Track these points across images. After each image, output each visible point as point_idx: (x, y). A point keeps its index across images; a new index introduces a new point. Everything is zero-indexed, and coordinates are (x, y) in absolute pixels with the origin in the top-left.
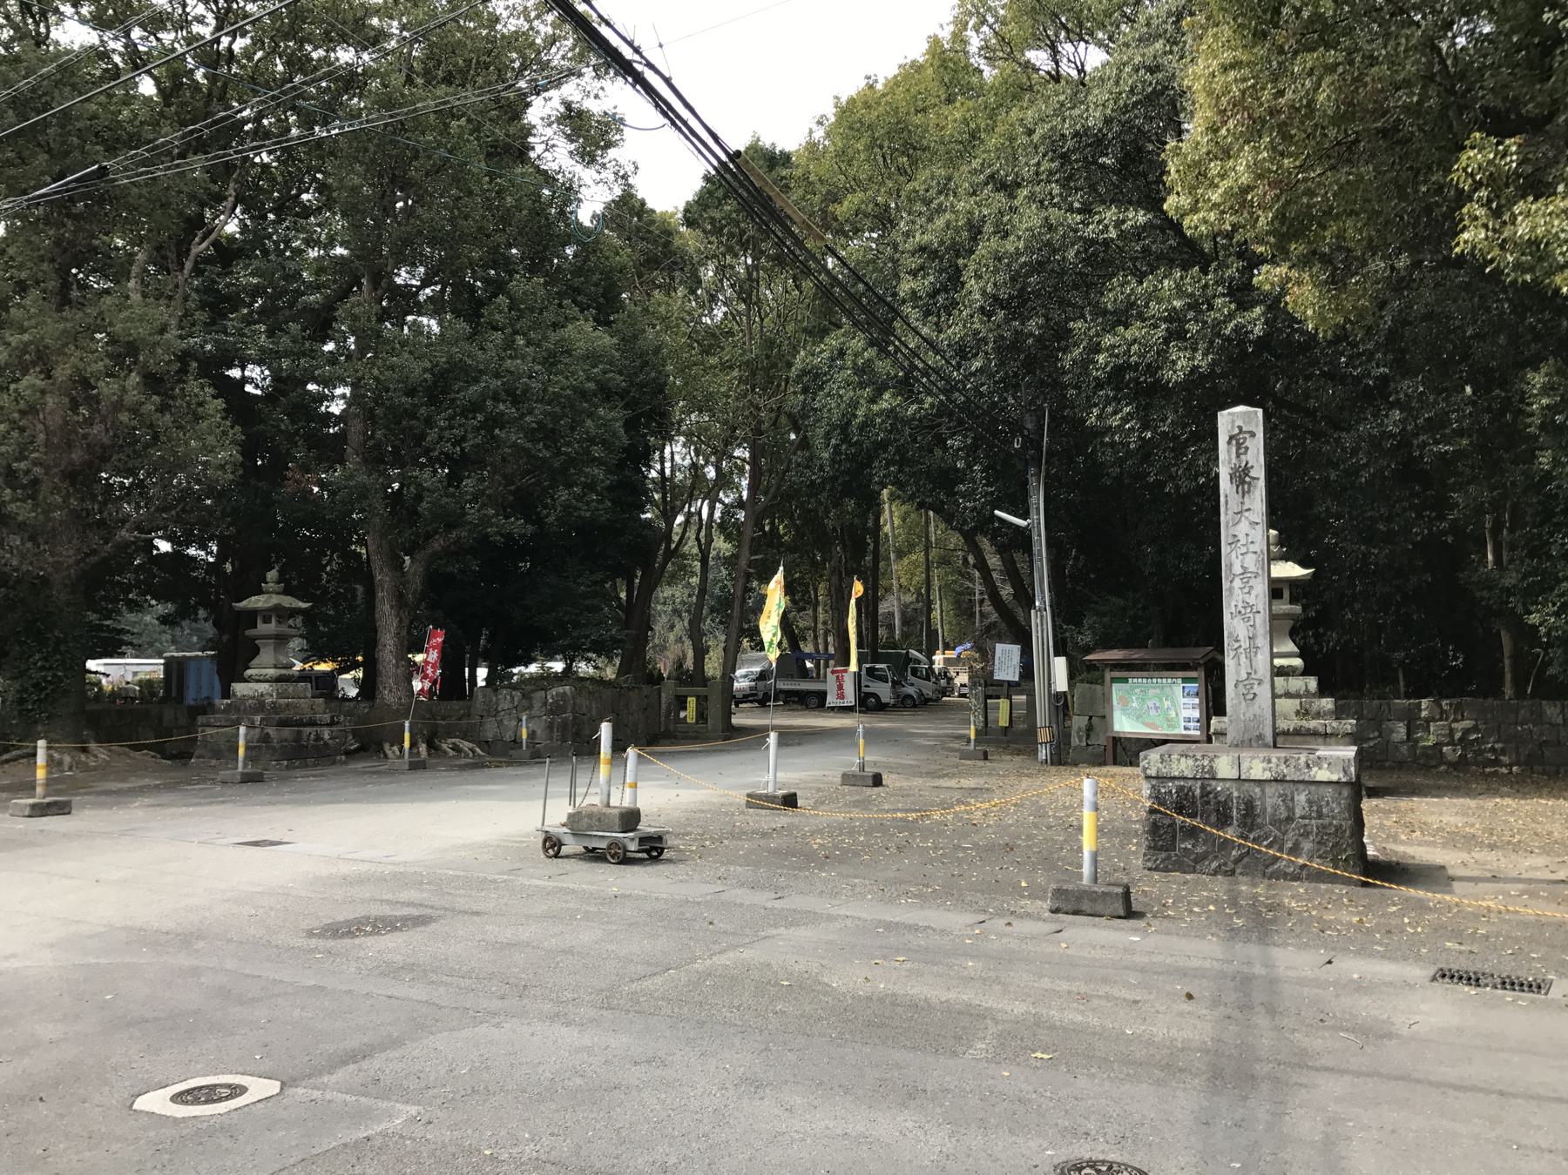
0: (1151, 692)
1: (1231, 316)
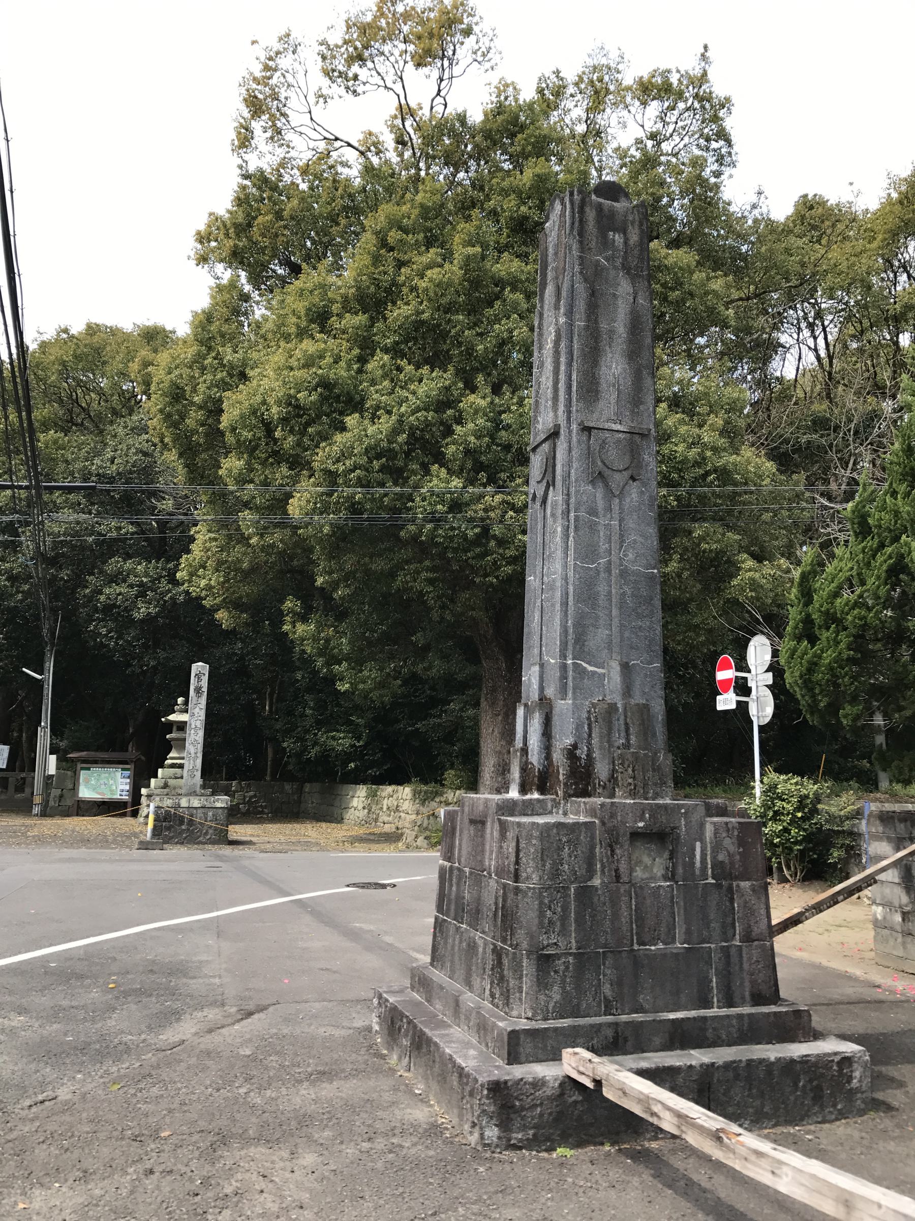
0: (103, 775)
1: (169, 591)
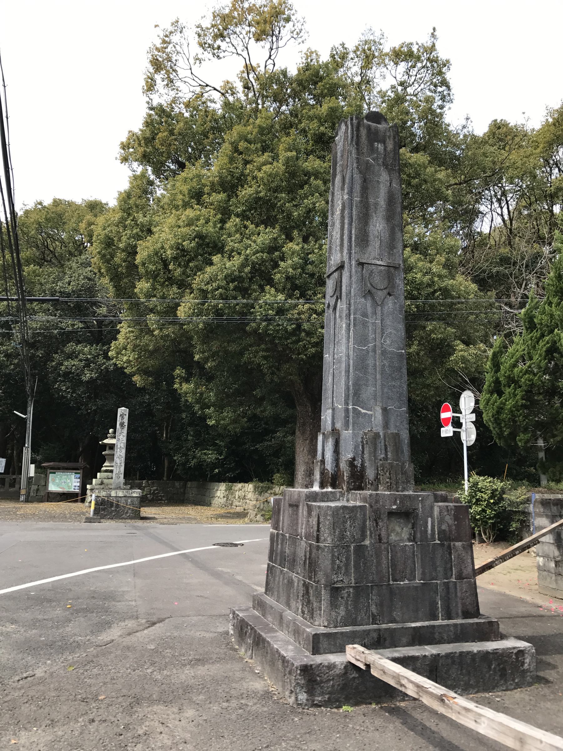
0: (63, 477)
1: (104, 363)
